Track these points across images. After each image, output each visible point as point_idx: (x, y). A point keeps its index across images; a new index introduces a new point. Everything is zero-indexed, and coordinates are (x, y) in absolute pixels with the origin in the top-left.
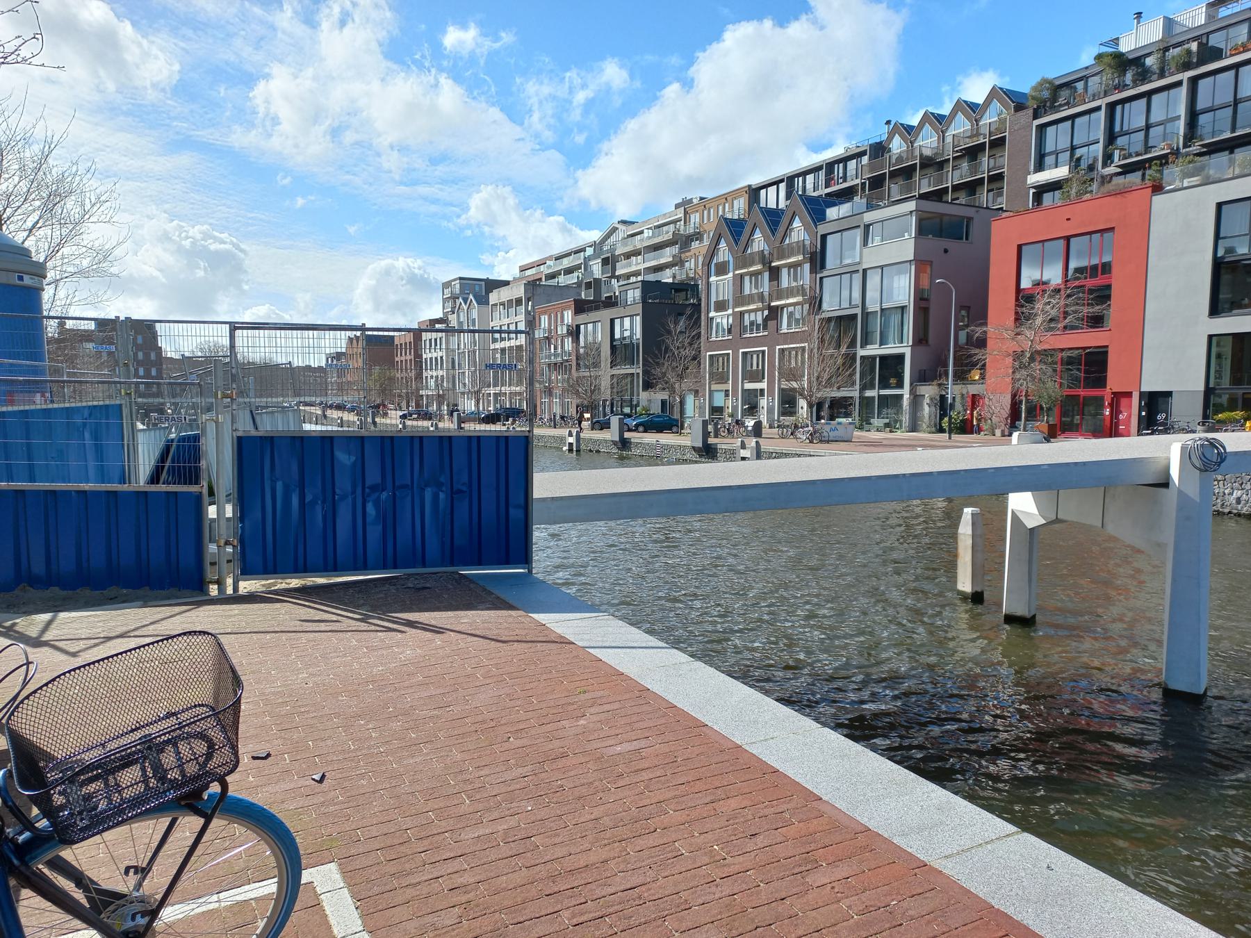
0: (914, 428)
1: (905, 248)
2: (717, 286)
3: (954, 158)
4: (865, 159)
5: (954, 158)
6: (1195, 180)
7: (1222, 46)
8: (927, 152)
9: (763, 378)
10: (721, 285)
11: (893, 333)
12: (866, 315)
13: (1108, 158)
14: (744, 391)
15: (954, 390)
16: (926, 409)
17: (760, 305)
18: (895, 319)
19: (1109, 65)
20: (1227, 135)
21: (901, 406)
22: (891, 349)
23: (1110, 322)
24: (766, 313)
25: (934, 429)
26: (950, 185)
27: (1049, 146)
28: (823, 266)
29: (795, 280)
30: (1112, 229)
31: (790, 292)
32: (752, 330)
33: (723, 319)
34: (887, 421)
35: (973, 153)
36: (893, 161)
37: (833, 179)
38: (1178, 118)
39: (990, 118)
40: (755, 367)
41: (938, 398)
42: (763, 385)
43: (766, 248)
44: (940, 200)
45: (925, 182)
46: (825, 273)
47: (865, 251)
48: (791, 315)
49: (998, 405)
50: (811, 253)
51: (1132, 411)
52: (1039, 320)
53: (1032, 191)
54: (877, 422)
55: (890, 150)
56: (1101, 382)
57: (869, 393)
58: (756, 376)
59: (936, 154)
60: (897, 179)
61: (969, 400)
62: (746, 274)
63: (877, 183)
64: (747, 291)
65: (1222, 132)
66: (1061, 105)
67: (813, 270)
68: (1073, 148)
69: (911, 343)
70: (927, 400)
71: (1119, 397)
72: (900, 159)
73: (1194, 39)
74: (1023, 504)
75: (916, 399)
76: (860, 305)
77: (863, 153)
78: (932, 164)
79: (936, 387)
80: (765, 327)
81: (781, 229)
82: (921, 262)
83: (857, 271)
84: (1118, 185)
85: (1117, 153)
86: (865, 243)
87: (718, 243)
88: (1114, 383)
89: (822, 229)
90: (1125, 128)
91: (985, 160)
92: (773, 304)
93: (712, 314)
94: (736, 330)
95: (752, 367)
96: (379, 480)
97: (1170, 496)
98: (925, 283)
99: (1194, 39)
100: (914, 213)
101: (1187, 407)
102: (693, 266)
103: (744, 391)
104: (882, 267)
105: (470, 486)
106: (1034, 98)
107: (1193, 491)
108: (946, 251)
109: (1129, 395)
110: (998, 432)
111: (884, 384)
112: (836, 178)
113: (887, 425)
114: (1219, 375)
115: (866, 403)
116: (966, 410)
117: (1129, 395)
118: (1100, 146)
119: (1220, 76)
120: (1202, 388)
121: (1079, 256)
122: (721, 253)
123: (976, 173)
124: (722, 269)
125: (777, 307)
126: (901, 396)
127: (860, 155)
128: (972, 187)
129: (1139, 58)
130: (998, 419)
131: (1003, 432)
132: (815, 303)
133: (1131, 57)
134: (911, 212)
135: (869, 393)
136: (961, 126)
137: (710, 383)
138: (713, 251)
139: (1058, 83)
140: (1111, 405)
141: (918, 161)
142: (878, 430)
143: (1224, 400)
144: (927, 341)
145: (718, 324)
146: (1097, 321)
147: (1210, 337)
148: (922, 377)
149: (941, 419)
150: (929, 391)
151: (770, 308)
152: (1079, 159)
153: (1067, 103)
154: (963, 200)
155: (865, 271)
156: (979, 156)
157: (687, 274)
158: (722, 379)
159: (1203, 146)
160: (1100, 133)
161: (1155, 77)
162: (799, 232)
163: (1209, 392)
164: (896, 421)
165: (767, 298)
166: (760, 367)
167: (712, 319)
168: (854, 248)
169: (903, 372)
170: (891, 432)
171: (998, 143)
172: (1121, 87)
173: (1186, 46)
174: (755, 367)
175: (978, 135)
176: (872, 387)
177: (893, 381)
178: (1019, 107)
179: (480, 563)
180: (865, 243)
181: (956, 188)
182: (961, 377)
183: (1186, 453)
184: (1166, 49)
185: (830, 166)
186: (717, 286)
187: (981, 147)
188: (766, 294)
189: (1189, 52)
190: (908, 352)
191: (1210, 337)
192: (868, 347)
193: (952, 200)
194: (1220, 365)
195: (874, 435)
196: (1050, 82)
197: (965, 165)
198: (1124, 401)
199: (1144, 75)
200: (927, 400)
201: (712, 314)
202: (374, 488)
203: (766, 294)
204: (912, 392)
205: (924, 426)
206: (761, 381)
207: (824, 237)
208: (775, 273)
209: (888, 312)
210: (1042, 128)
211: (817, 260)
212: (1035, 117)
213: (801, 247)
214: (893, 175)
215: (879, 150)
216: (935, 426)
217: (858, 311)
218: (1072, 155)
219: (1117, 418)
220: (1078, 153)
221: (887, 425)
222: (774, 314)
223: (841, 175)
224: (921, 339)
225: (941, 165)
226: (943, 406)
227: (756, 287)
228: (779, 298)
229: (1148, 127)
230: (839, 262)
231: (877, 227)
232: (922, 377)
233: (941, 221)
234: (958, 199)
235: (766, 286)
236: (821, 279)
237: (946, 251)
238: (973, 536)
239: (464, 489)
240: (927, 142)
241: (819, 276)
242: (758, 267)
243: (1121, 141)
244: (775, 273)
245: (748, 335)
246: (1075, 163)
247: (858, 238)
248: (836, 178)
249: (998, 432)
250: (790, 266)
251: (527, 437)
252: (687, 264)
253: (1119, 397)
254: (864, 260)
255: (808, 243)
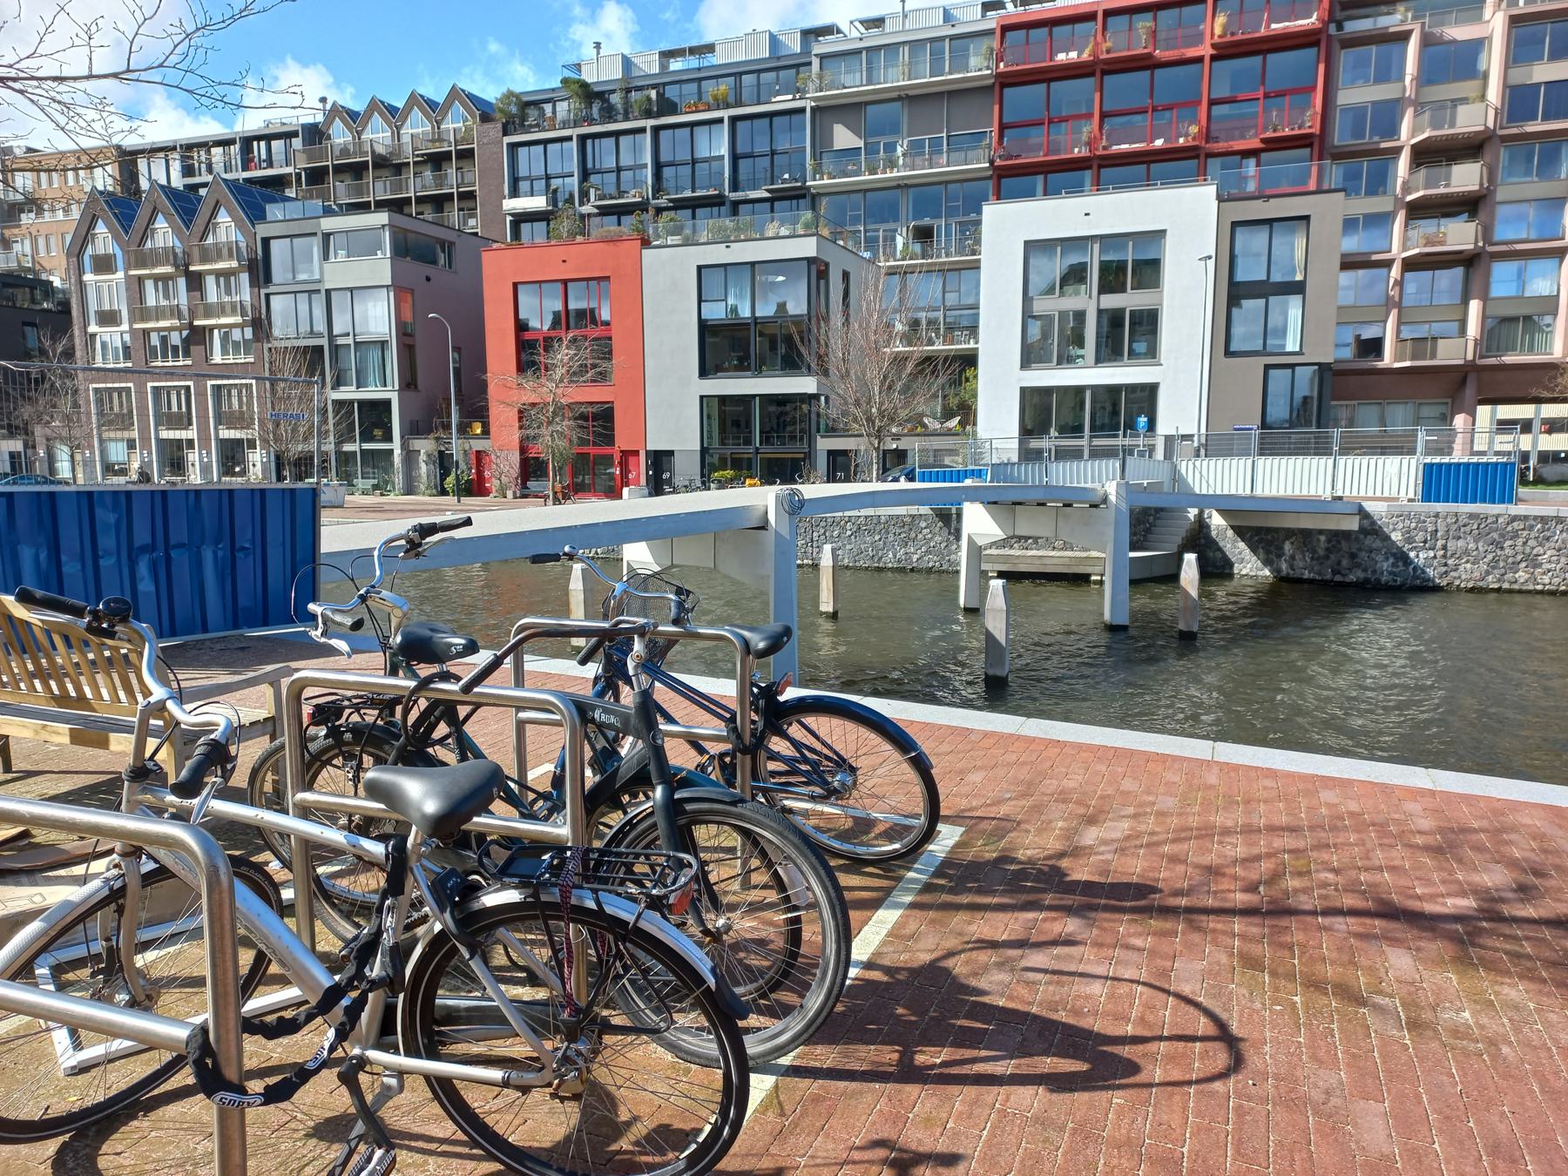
0: (410, 490)
1: (380, 268)
2: (98, 290)
3: (415, 163)
4: (297, 143)
5: (415, 163)
6: (675, 239)
7: (676, 100)
8: (380, 150)
9: (190, 424)
10: (106, 289)
11: (373, 374)
12: (336, 349)
13: (584, 195)
14: (160, 441)
15: (457, 447)
16: (423, 467)
17: (176, 322)
18: (374, 355)
19: (577, 94)
20: (688, 194)
21: (392, 464)
22: (372, 393)
23: (614, 378)
24: (185, 333)
25: (434, 491)
26: (371, 199)
27: (523, 171)
28: (268, 279)
29: (228, 292)
30: (607, 278)
31: (221, 310)
32: (165, 356)
33: (113, 336)
34: (375, 482)
35: (437, 161)
36: (337, 153)
37: (252, 160)
38: (645, 166)
39: (454, 123)
40: (175, 408)
41: (436, 454)
42: (191, 433)
43: (178, 244)
44: (401, 212)
45: (379, 185)
46: (272, 289)
47: (326, 266)
48: (225, 339)
49: (506, 463)
50: (250, 260)
51: (641, 468)
52: (560, 372)
53: (509, 218)
54: (360, 482)
55: (329, 138)
56: (609, 439)
57: (348, 447)
58: (183, 421)
59: (391, 153)
60: (342, 177)
61: (473, 457)
62: (149, 277)
63: (316, 176)
64: (151, 301)
65: (684, 189)
66: (531, 126)
67: (255, 283)
68: (548, 178)
69: (397, 387)
70: (423, 457)
71: (628, 455)
72: (345, 152)
73: (654, 86)
74: (638, 555)
75: (410, 456)
76: (326, 334)
77: (294, 134)
78: (387, 165)
79: (433, 442)
80: (187, 354)
81: (200, 220)
82: (400, 289)
83: (318, 291)
84: (609, 231)
85: (592, 191)
86: (326, 257)
87: (92, 225)
88: (622, 441)
89: (262, 230)
90: (597, 166)
91: (451, 172)
92: (196, 323)
93: (93, 328)
94: (139, 354)
95: (170, 407)
96: (149, 541)
97: (769, 537)
98: (408, 316)
99: (654, 86)
100: (387, 228)
101: (686, 467)
102: (28, 250)
103: (160, 441)
104: (351, 290)
105: (253, 542)
106: (501, 111)
107: (785, 532)
108: (428, 279)
109: (636, 453)
110: (510, 494)
111: (367, 436)
112: (256, 159)
113: (375, 487)
114: (710, 437)
115: (345, 459)
116: (470, 469)
117: (636, 453)
118: (575, 179)
119: (756, 122)
120: (698, 448)
121: (577, 298)
122: (99, 242)
123: (441, 186)
124: (104, 264)
125: (204, 327)
126: (391, 451)
127: (288, 136)
128: (439, 202)
129: (603, 93)
130: (507, 480)
131: (514, 493)
132: (260, 325)
133: (596, 89)
134: (383, 226)
135: (348, 447)
136: (417, 126)
137: (99, 427)
138: (84, 236)
139: (526, 99)
140: (621, 464)
141: (369, 158)
142: (363, 493)
143: (715, 460)
144: (416, 387)
145: (104, 345)
146: (603, 377)
147: (702, 397)
148: (414, 429)
149: (443, 480)
150: (424, 447)
151: (191, 326)
152: (555, 191)
153: (538, 125)
154: (429, 216)
155: (328, 292)
156: (444, 166)
157: (19, 262)
158: (124, 421)
159: (670, 200)
160: (574, 166)
161: (620, 117)
162: (227, 228)
163: (704, 451)
164: (387, 483)
165: (186, 313)
166: (184, 409)
167: (93, 336)
168: (311, 261)
169: (390, 421)
170: (382, 495)
171: (466, 155)
172: (591, 122)
173: (645, 92)
174: (175, 408)
175: (440, 140)
176: (352, 440)
177: (378, 432)
178: (486, 118)
179: (266, 623)
180: (326, 257)
181: (421, 200)
182: (464, 430)
183: (779, 500)
184: (628, 91)
185: (247, 142)
186: (98, 290)
187: (446, 156)
188: (185, 309)
189: (649, 99)
190: (395, 398)
191: (702, 397)
192: (342, 388)
193: (417, 214)
194: (709, 425)
195: (358, 499)
196: (517, 96)
197: (428, 174)
198: (632, 460)
199: (609, 114)
200: (423, 457)
201: (93, 328)
202: (144, 549)
203: (185, 309)
204: (404, 446)
205: (422, 487)
206: (186, 429)
207: (266, 242)
208: (195, 282)
209: (363, 347)
210: (513, 147)
211: (260, 269)
212: (505, 133)
213: (232, 250)
214: (339, 170)
215: (314, 134)
216: (436, 487)
217: (324, 342)
218: (548, 186)
219: (627, 477)
220: (555, 183)
221: (375, 487)
222: (197, 337)
223: (264, 156)
224: (409, 383)
225: (399, 168)
226: (444, 462)
227: (166, 296)
228: (207, 316)
229: (619, 170)
230: (291, 276)
231: (341, 239)
232: (414, 429)
233: (406, 239)
234: (422, 213)
235: (182, 297)
236: (268, 296)
237: (428, 279)
238: (585, 591)
239: (247, 545)
240: (378, 135)
241: (263, 292)
242: (168, 269)
243: (594, 179)
244: (195, 282)
245: (160, 364)
246: (553, 196)
247: (315, 249)
248: (256, 159)
249: (510, 494)
250: (218, 274)
251: (314, 490)
252: (17, 247)
253: (628, 455)
254: (326, 277)
255: (243, 245)
